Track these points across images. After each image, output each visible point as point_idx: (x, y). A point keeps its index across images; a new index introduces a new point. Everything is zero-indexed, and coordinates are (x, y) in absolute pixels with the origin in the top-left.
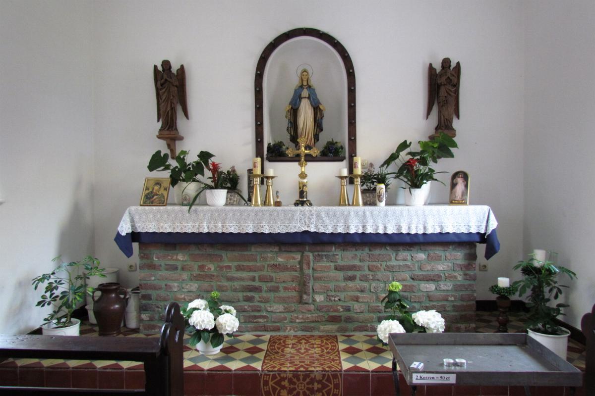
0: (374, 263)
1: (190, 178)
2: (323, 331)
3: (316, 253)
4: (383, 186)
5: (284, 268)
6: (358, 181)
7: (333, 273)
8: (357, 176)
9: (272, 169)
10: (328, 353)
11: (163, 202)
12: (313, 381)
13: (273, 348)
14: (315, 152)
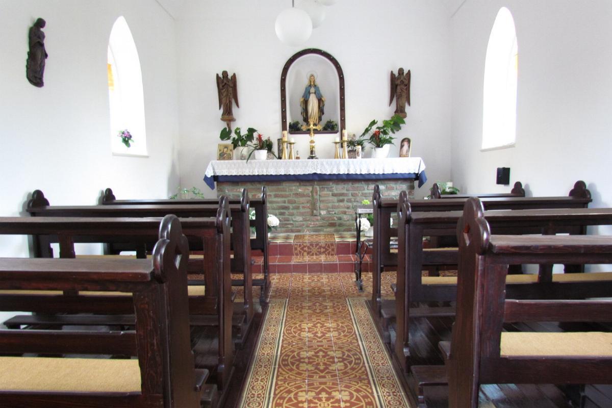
0: (355, 192)
1: (244, 145)
2: (326, 232)
3: (321, 186)
4: (360, 147)
5: (302, 195)
6: (345, 145)
7: (331, 198)
8: (344, 141)
9: (294, 138)
10: (345, 336)
11: (230, 158)
12: (321, 247)
13: (290, 332)
14: (319, 127)
